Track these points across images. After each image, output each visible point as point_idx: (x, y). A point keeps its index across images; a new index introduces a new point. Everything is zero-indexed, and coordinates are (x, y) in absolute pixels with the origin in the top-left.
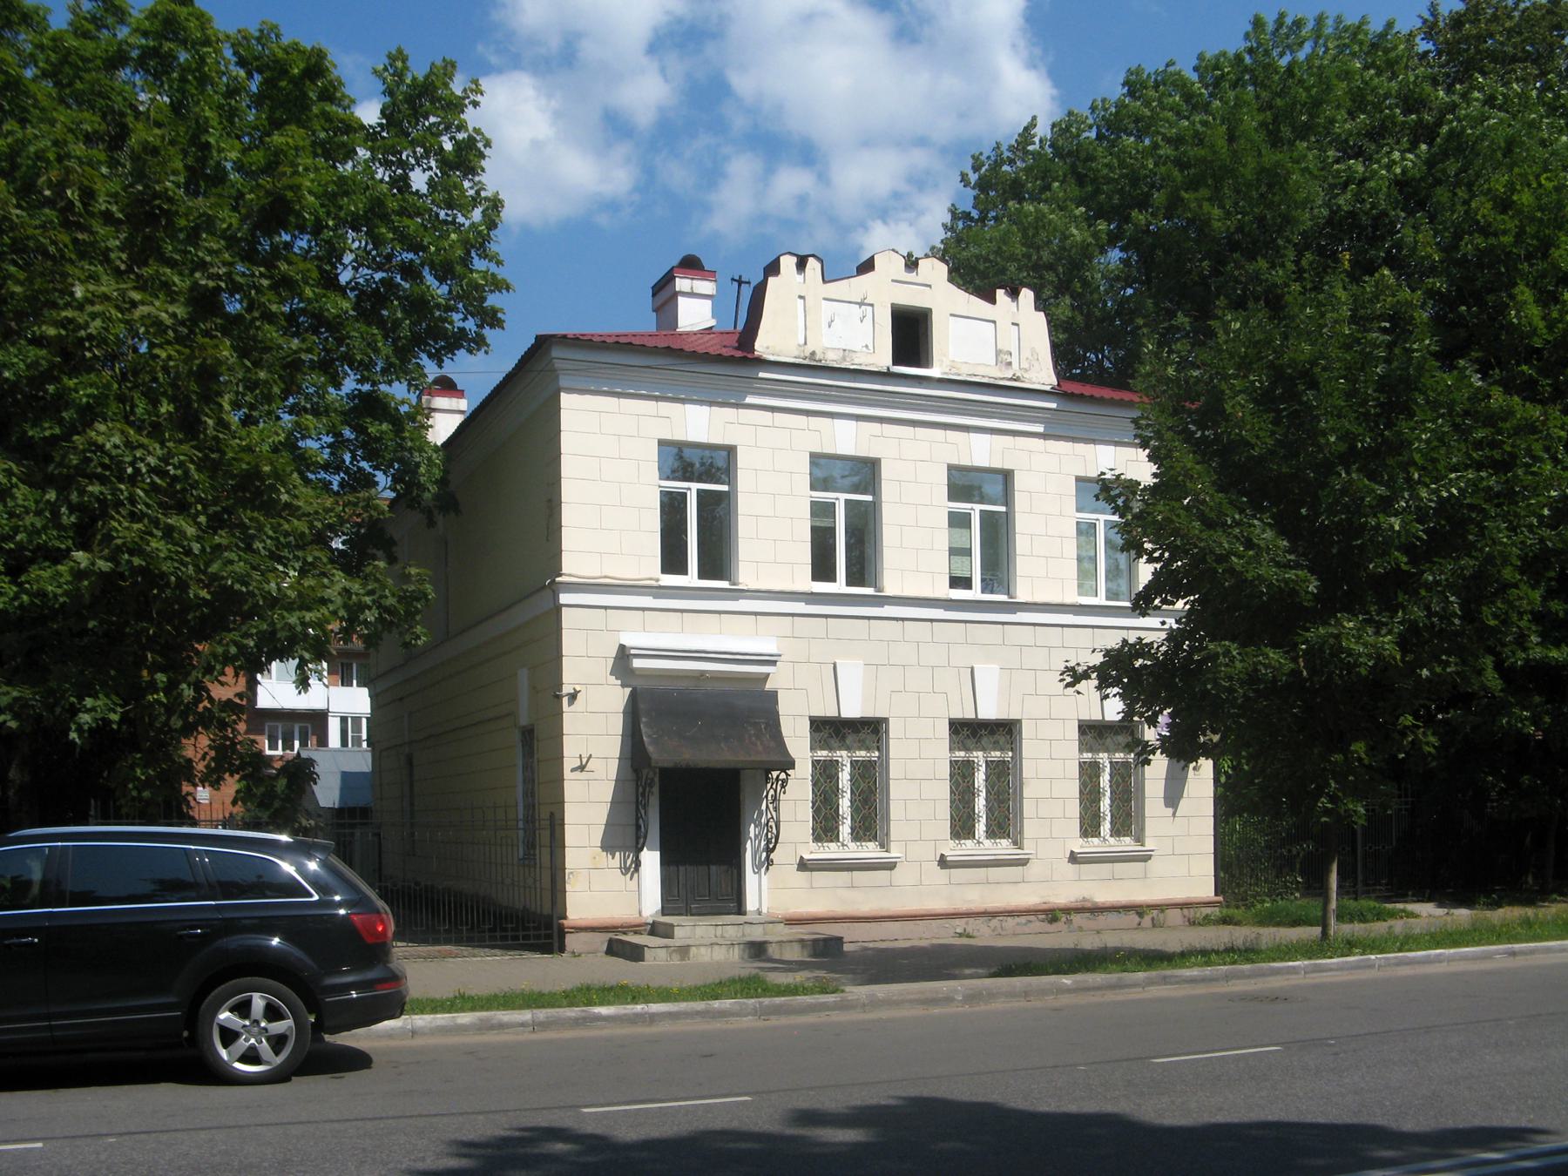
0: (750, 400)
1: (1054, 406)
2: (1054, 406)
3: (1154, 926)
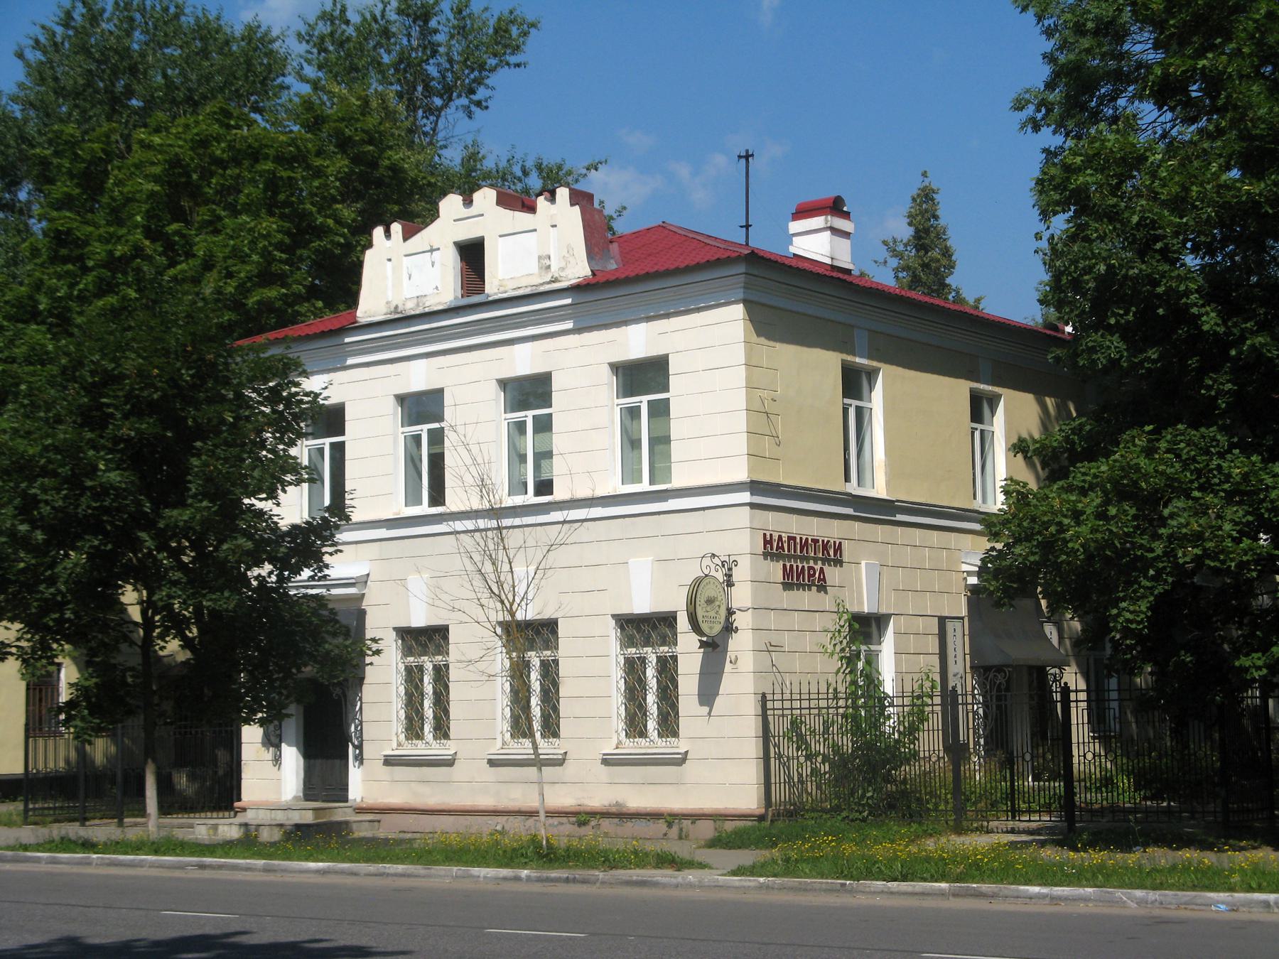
0: (350, 361)
1: (569, 301)
2: (569, 301)
3: (680, 838)
